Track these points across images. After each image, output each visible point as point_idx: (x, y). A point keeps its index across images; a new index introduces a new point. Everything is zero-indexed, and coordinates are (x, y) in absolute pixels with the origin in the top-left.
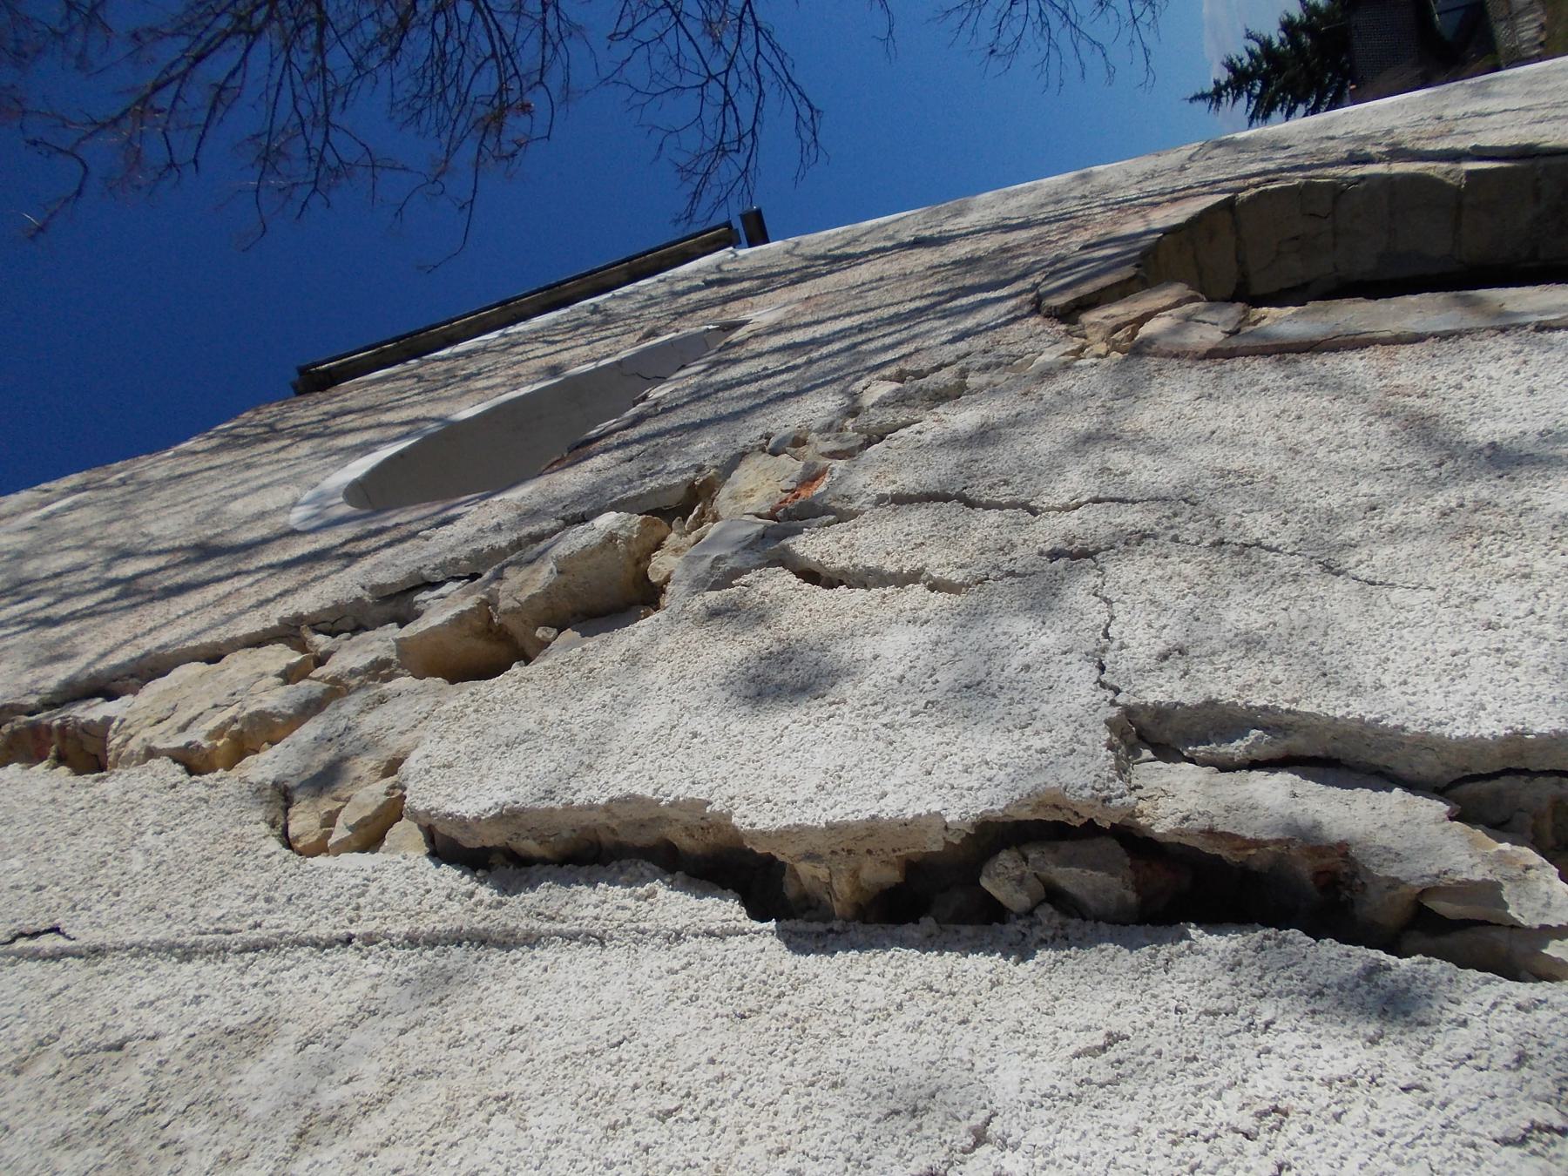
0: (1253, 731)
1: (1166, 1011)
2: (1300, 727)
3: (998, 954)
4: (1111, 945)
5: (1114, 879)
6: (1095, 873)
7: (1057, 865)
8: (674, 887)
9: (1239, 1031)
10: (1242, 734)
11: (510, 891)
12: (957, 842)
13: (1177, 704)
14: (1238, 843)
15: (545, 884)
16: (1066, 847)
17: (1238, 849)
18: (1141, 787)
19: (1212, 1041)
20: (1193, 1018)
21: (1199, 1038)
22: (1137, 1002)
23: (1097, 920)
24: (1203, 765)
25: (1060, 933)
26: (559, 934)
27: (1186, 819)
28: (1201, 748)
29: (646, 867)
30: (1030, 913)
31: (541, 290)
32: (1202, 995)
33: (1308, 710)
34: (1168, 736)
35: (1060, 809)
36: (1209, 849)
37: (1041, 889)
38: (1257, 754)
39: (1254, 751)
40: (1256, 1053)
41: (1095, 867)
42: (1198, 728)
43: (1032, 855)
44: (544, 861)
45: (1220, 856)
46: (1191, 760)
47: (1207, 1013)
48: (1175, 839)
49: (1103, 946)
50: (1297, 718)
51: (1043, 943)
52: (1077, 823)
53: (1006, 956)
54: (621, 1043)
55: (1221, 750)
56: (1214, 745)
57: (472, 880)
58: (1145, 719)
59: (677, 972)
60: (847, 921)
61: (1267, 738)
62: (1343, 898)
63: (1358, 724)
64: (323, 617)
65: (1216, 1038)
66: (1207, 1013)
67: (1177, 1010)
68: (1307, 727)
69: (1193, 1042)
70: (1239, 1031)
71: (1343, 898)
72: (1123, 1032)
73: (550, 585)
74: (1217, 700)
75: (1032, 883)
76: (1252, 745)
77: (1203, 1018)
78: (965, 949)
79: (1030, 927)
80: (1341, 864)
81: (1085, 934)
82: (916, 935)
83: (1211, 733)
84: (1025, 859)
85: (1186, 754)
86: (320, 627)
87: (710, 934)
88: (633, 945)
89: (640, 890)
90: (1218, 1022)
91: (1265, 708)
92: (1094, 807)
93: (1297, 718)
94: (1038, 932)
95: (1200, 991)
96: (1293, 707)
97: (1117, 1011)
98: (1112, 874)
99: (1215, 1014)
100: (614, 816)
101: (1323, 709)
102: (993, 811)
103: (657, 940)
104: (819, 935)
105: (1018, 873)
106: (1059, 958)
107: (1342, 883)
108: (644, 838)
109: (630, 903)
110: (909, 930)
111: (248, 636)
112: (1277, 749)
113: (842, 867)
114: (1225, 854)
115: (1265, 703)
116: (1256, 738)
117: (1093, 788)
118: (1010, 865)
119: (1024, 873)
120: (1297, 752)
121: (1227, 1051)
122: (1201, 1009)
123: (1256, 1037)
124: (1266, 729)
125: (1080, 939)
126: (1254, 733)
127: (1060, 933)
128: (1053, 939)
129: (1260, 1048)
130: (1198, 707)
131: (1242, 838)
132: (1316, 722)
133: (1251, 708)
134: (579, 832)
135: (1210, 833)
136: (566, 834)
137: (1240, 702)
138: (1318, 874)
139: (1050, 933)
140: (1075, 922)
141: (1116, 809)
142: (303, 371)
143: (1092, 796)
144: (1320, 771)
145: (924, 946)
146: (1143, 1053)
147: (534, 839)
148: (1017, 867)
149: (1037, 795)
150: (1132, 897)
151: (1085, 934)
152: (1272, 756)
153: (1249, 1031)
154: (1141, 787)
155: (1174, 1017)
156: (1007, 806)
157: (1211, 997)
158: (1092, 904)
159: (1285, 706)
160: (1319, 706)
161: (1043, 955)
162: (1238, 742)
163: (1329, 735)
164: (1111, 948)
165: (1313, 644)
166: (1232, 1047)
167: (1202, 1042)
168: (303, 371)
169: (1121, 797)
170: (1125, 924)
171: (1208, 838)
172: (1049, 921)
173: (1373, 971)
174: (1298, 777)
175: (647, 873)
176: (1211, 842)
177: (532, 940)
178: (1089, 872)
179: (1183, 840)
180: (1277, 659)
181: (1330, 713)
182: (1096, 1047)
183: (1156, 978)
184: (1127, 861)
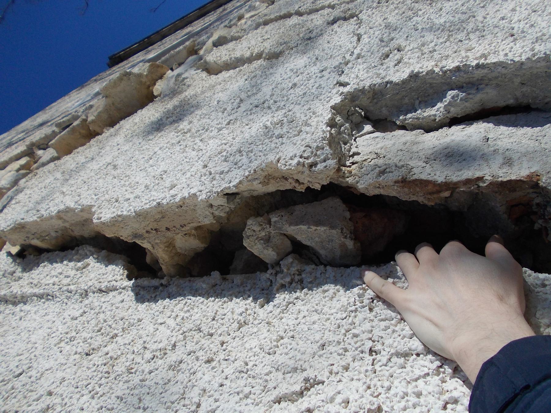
0: (450, 92)
1: (362, 352)
2: (490, 80)
3: (251, 299)
4: (332, 286)
5: (334, 231)
6: (318, 228)
7: (291, 224)
8: (98, 260)
9: (428, 374)
10: (441, 97)
11: (27, 270)
12: (223, 214)
13: (387, 82)
14: (430, 187)
15: (43, 264)
16: (299, 209)
17: (431, 193)
18: (358, 154)
19: (399, 387)
20: (384, 360)
21: (386, 384)
22: (339, 343)
23: (325, 266)
24: (412, 130)
25: (297, 278)
26: (35, 295)
27: (383, 172)
28: (409, 116)
29: (88, 249)
30: (278, 264)
31: (196, 10)
32: (396, 335)
33: (495, 60)
34: (385, 111)
35: (286, 179)
36: (405, 195)
37: (288, 243)
38: (455, 112)
39: (452, 109)
40: (441, 403)
41: (318, 223)
42: (406, 100)
43: (274, 219)
44: (48, 251)
45: (417, 201)
46: (403, 127)
47: (398, 354)
48: (377, 192)
49: (326, 287)
50: (486, 71)
51: (283, 287)
52: (300, 189)
53: (255, 300)
54: (21, 374)
55: (425, 114)
56: (419, 112)
57: (15, 265)
58: (365, 101)
59: (76, 319)
60: (172, 277)
61: (462, 95)
62: (537, 226)
63: (543, 64)
64: (42, 142)
65: (404, 383)
66: (398, 354)
67: (371, 351)
68: (496, 78)
69: (380, 390)
70: (428, 374)
71: (537, 226)
72: (319, 378)
73: (106, 106)
74: (419, 73)
75: (277, 240)
76: (450, 104)
77: (394, 359)
78: (231, 295)
79: (276, 274)
80: (534, 195)
81: (316, 278)
82: (204, 286)
83: (417, 102)
84: (269, 223)
85: (398, 123)
86: (41, 147)
87: (101, 291)
88: (66, 300)
89: (79, 264)
90: (409, 364)
91: (458, 69)
92: (303, 173)
93: (486, 71)
94: (280, 280)
95: (394, 331)
96: (482, 61)
97: (321, 352)
98: (332, 227)
99: (406, 355)
100: (65, 221)
101: (510, 56)
102: (229, 187)
103: (77, 297)
104: (156, 288)
105: (263, 234)
106: (291, 300)
107: (535, 213)
108: (86, 233)
109: (72, 273)
110: (202, 283)
111: (16, 156)
112: (470, 106)
113: (157, 241)
114: (421, 199)
115: (457, 64)
116: (453, 97)
117: (301, 157)
118: (257, 228)
119: (270, 233)
120: (491, 105)
121: (413, 399)
122: (393, 351)
123: (444, 381)
124: (460, 88)
125: (311, 282)
126: (451, 93)
127: (297, 278)
128: (291, 283)
129: (446, 397)
130: (404, 82)
131: (433, 183)
132: (504, 71)
133: (446, 72)
134: (60, 232)
135: (404, 182)
136: (53, 234)
137: (437, 70)
138: (512, 207)
139: (288, 279)
140: (309, 268)
141: (321, 172)
142: (110, 58)
143: (299, 163)
144: (513, 117)
145: (207, 294)
146: (332, 400)
147: (38, 239)
148: (263, 229)
149: (262, 170)
150: (350, 244)
151: (316, 278)
152: (469, 111)
153: (438, 375)
154: (358, 154)
155: (368, 359)
156: (240, 182)
157: (404, 337)
158: (322, 252)
159: (474, 63)
160: (506, 55)
161: (281, 298)
162: (439, 105)
163: (517, 80)
164: (331, 288)
165: (503, 19)
166: (419, 395)
167: (389, 389)
168: (110, 58)
169: (325, 161)
170: (347, 266)
171: (403, 187)
172: (288, 269)
173: (486, 59)
174: (491, 125)
175: (88, 253)
176: (406, 190)
177: (24, 300)
178: (314, 228)
179: (382, 192)
180: (472, 36)
181: (517, 59)
182: (293, 393)
183: (360, 316)
184: (348, 215)
